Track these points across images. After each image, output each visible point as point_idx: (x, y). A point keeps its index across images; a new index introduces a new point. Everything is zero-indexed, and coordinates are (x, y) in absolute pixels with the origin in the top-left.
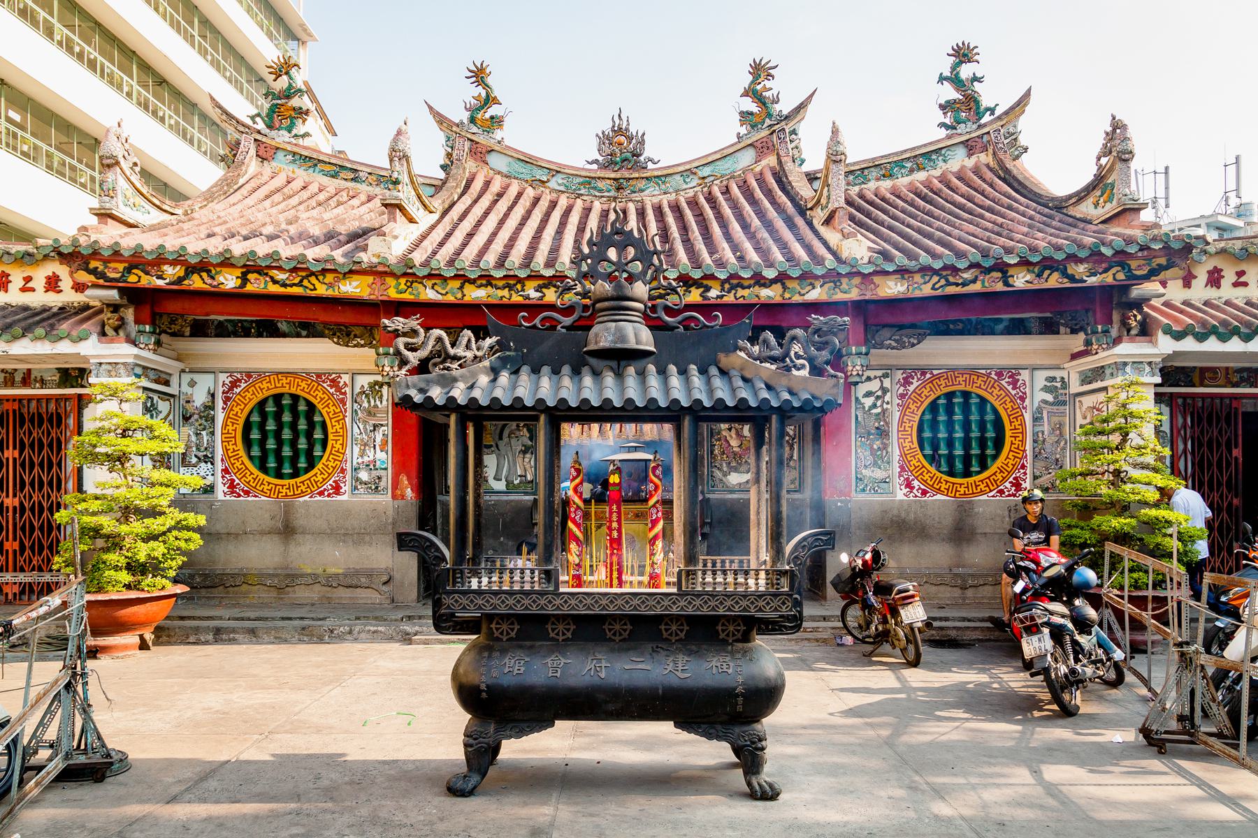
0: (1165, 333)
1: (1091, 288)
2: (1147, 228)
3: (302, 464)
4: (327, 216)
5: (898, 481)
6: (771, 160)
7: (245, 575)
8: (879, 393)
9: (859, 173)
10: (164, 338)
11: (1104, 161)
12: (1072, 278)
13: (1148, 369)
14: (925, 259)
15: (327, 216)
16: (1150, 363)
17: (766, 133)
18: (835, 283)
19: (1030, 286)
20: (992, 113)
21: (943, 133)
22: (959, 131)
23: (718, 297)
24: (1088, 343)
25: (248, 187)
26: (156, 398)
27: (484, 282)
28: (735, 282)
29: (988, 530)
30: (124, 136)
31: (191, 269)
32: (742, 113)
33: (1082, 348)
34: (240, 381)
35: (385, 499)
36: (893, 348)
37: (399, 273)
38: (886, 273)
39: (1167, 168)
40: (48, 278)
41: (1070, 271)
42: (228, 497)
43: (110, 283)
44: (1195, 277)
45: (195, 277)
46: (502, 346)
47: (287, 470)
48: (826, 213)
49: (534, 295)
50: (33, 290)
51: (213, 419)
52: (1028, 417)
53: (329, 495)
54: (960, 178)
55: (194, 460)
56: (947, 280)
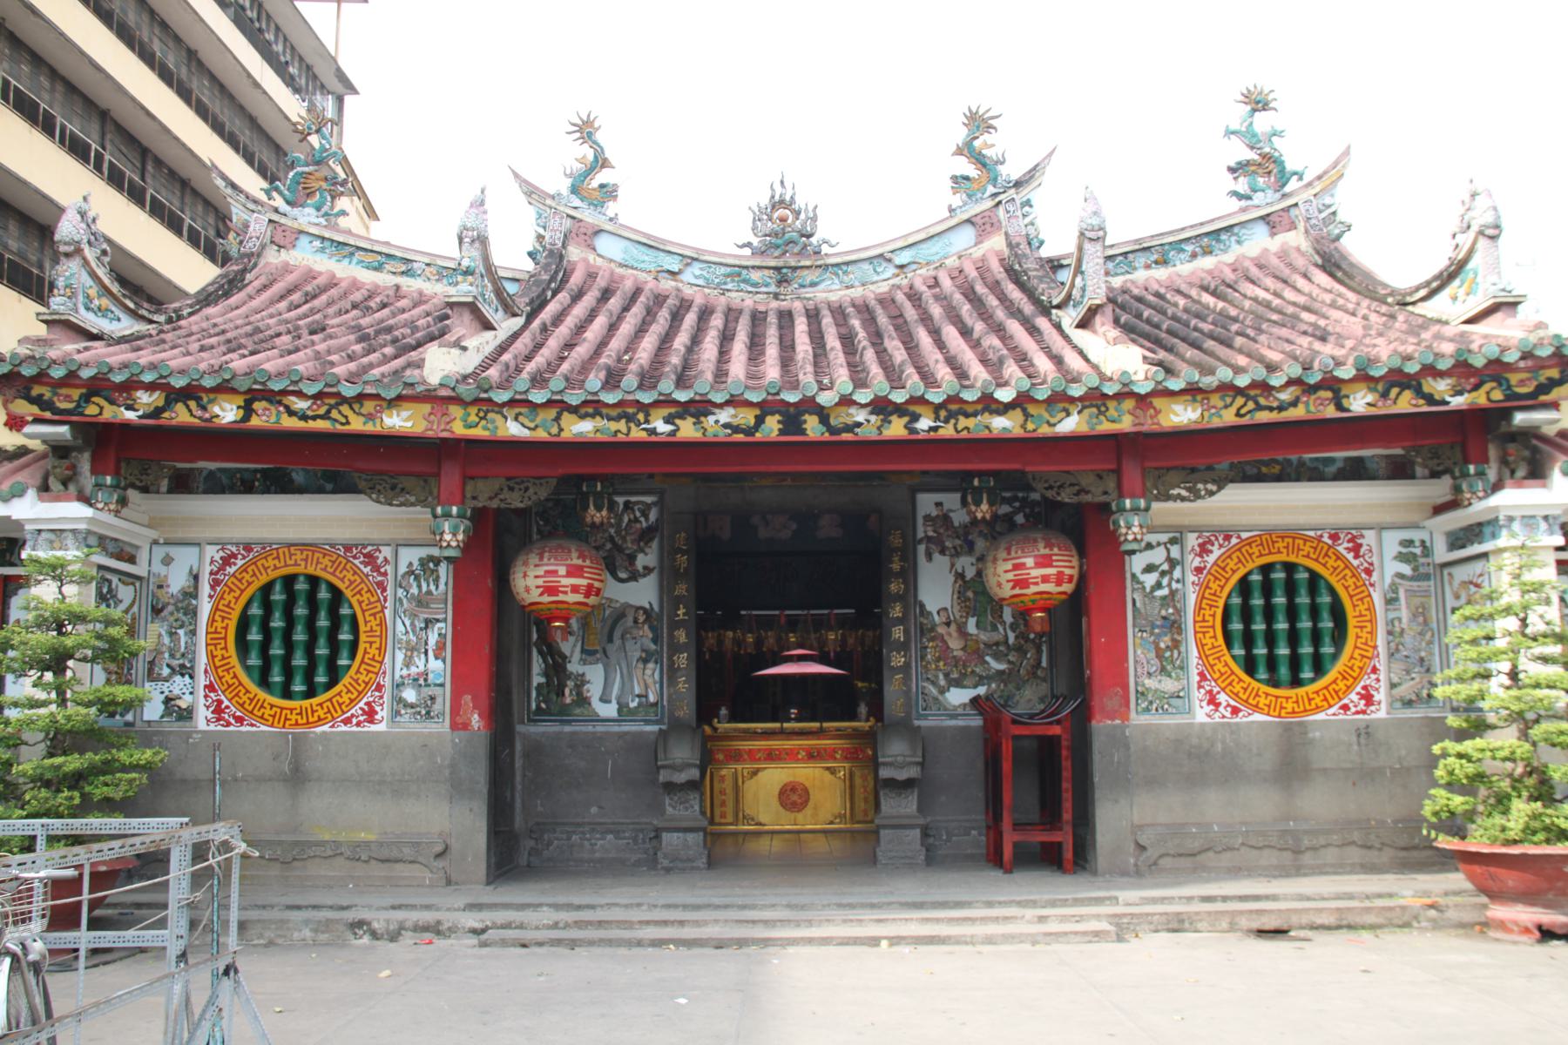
1: (1458, 414)
4: (365, 322)
5: (1197, 695)
6: (997, 243)
8: (1165, 567)
9: (1121, 259)
10: (132, 494)
11: (1460, 238)
12: (1430, 399)
13: (1543, 525)
14: (1224, 374)
15: (365, 322)
16: (1546, 518)
17: (989, 204)
18: (1098, 407)
19: (1373, 411)
20: (1301, 178)
21: (1236, 204)
22: (1256, 202)
23: (932, 429)
24: (1457, 489)
26: (115, 580)
27: (590, 410)
28: (954, 407)
29: (1328, 765)
30: (91, 214)
32: (955, 179)
33: (1449, 498)
34: (234, 556)
35: (442, 727)
36: (1183, 499)
37: (468, 399)
38: (1171, 394)
41: (1426, 389)
42: (212, 727)
43: (60, 417)
45: (180, 407)
47: (298, 687)
48: (1082, 310)
49: (662, 427)
53: (358, 724)
54: (1260, 267)
55: (166, 671)
56: (1257, 403)
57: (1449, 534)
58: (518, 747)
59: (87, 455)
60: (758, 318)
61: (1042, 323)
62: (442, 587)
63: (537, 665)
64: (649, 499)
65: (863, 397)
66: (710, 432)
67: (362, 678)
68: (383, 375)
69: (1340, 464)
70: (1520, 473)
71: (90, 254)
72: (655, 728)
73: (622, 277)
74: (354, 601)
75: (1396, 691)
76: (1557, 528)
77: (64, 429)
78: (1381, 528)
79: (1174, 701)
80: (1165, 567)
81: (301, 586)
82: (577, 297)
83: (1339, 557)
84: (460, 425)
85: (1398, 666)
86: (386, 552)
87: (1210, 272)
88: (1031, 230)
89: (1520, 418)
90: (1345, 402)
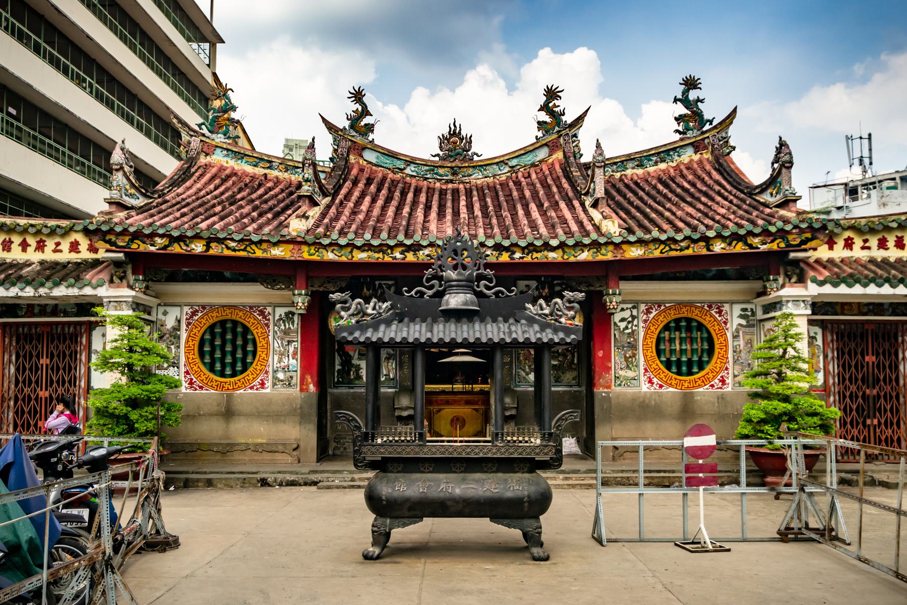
0: (812, 281)
2: (799, 213)
3: (239, 367)
6: (559, 155)
7: (199, 444)
8: (630, 319)
10: (150, 283)
11: (776, 166)
13: (802, 305)
14: (655, 233)
16: (804, 301)
17: (555, 136)
19: (724, 251)
20: (711, 124)
21: (677, 137)
23: (521, 258)
25: (197, 174)
31: (174, 240)
32: (539, 123)
35: (295, 391)
38: (629, 243)
39: (870, 135)
40: (72, 243)
41: (749, 242)
42: (188, 391)
43: (120, 249)
44: (836, 243)
45: (176, 245)
46: (393, 307)
47: (228, 371)
49: (398, 255)
50: (61, 251)
51: (179, 338)
52: (729, 335)
54: (688, 168)
57: (764, 306)
58: (329, 399)
59: (130, 266)
60: (443, 193)
61: (576, 203)
62: (295, 325)
63: (338, 361)
64: (390, 283)
65: (490, 243)
66: (421, 258)
67: (258, 368)
68: (271, 231)
69: (713, 273)
70: (793, 280)
71: (127, 169)
72: (393, 390)
73: (376, 171)
74: (254, 332)
75: (736, 379)
76: (809, 307)
77: (121, 255)
78: (732, 303)
79: (633, 381)
80: (630, 319)
81: (229, 325)
82: (355, 183)
83: (711, 316)
84: (306, 254)
85: (737, 367)
86: (269, 309)
87: (663, 171)
88: (577, 150)
89: (792, 255)
90: (711, 247)
